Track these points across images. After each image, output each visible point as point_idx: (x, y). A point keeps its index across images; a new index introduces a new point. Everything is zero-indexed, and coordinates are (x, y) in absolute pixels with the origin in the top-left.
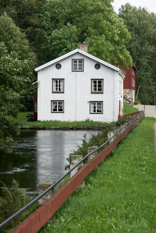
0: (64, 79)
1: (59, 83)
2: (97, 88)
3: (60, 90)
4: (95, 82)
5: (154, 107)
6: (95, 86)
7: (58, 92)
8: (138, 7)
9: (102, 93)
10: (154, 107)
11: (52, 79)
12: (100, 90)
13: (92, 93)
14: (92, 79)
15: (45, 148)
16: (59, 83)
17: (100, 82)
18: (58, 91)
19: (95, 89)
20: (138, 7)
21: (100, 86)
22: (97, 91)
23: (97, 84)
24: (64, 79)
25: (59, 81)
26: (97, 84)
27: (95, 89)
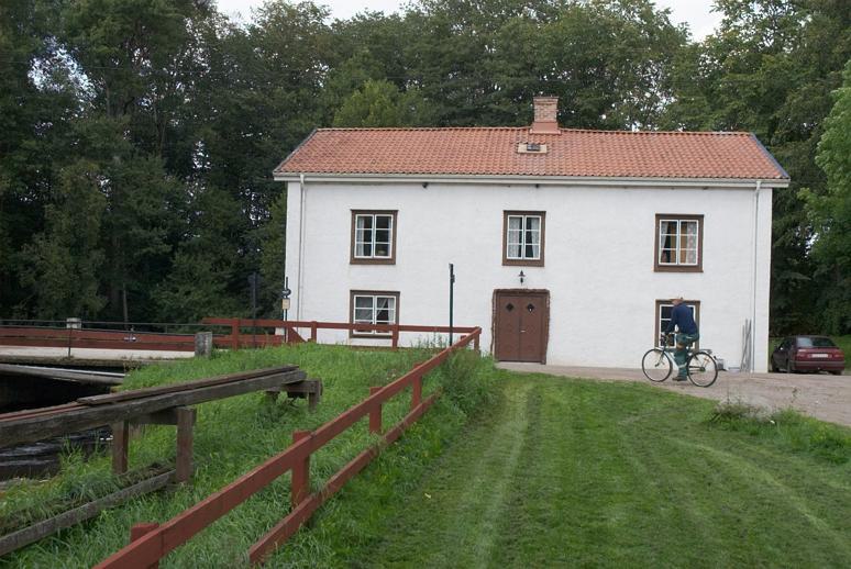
0: (702, 216)
1: (529, 226)
2: (374, 242)
3: (529, 252)
4: (368, 223)
5: (845, 380)
6: (367, 236)
7: (373, 259)
8: (402, 15)
9: (392, 262)
10: (844, 380)
11: (505, 212)
12: (383, 249)
13: (354, 261)
14: (659, 216)
15: (30, 456)
16: (529, 226)
17: (383, 222)
18: (523, 257)
19: (367, 250)
20: (402, 15)
21: (382, 236)
22: (373, 255)
23: (374, 229)
24: (702, 216)
25: (529, 221)
26: (374, 229)
27: (367, 250)
